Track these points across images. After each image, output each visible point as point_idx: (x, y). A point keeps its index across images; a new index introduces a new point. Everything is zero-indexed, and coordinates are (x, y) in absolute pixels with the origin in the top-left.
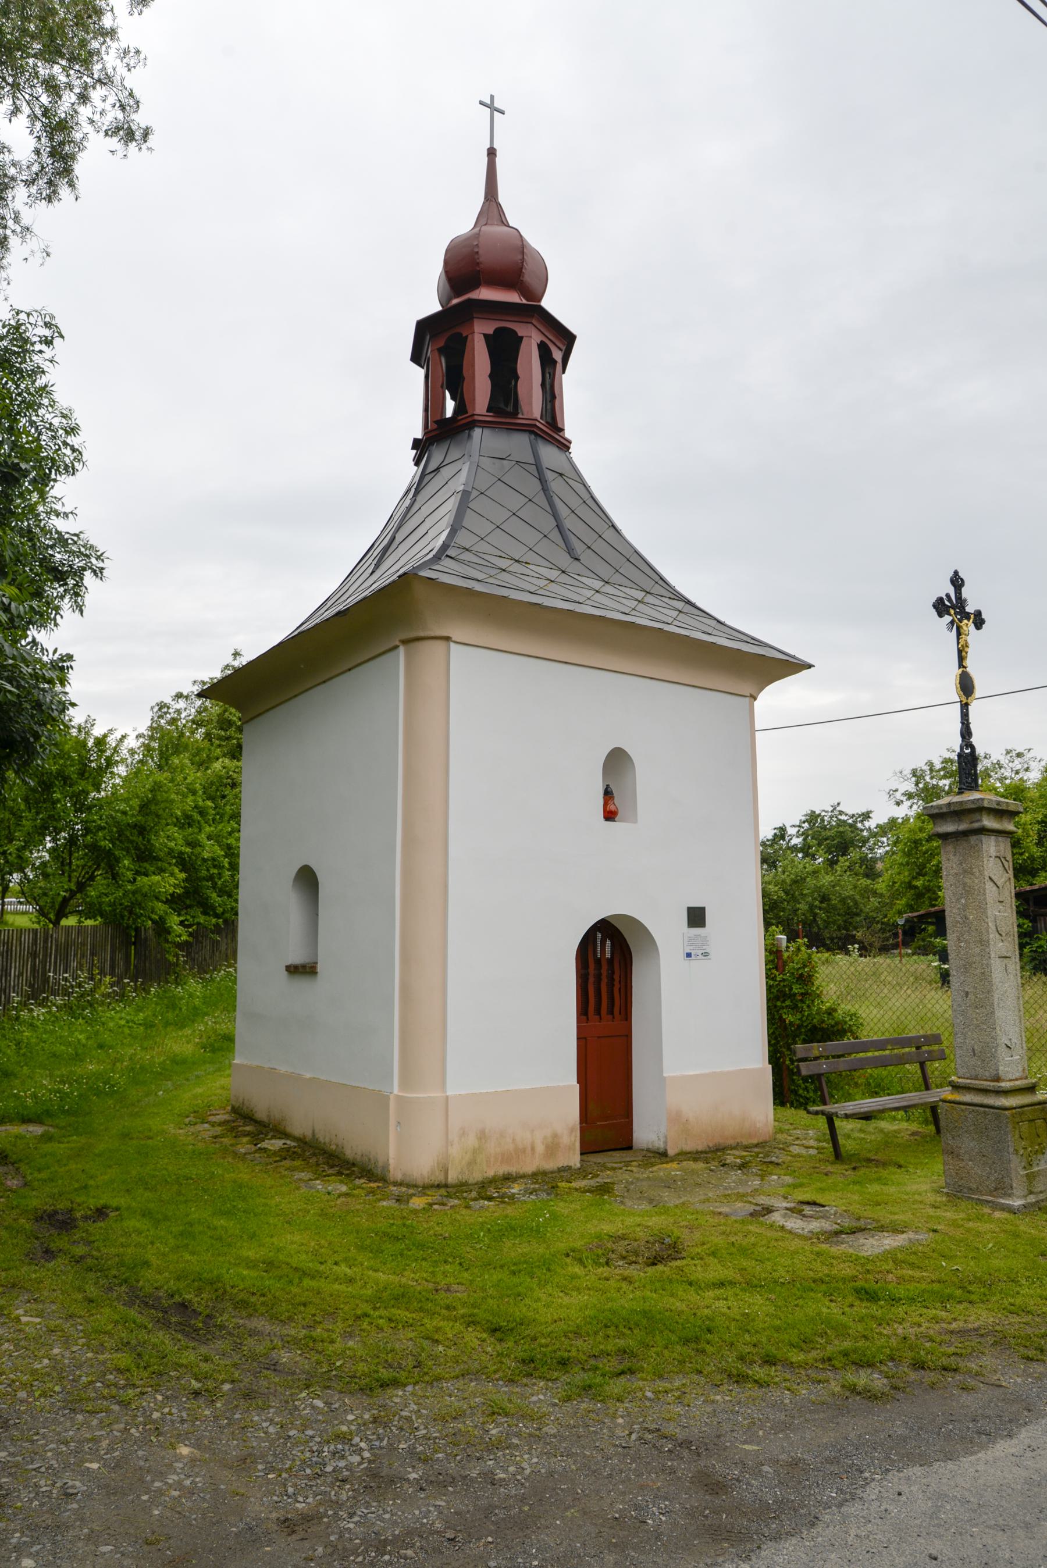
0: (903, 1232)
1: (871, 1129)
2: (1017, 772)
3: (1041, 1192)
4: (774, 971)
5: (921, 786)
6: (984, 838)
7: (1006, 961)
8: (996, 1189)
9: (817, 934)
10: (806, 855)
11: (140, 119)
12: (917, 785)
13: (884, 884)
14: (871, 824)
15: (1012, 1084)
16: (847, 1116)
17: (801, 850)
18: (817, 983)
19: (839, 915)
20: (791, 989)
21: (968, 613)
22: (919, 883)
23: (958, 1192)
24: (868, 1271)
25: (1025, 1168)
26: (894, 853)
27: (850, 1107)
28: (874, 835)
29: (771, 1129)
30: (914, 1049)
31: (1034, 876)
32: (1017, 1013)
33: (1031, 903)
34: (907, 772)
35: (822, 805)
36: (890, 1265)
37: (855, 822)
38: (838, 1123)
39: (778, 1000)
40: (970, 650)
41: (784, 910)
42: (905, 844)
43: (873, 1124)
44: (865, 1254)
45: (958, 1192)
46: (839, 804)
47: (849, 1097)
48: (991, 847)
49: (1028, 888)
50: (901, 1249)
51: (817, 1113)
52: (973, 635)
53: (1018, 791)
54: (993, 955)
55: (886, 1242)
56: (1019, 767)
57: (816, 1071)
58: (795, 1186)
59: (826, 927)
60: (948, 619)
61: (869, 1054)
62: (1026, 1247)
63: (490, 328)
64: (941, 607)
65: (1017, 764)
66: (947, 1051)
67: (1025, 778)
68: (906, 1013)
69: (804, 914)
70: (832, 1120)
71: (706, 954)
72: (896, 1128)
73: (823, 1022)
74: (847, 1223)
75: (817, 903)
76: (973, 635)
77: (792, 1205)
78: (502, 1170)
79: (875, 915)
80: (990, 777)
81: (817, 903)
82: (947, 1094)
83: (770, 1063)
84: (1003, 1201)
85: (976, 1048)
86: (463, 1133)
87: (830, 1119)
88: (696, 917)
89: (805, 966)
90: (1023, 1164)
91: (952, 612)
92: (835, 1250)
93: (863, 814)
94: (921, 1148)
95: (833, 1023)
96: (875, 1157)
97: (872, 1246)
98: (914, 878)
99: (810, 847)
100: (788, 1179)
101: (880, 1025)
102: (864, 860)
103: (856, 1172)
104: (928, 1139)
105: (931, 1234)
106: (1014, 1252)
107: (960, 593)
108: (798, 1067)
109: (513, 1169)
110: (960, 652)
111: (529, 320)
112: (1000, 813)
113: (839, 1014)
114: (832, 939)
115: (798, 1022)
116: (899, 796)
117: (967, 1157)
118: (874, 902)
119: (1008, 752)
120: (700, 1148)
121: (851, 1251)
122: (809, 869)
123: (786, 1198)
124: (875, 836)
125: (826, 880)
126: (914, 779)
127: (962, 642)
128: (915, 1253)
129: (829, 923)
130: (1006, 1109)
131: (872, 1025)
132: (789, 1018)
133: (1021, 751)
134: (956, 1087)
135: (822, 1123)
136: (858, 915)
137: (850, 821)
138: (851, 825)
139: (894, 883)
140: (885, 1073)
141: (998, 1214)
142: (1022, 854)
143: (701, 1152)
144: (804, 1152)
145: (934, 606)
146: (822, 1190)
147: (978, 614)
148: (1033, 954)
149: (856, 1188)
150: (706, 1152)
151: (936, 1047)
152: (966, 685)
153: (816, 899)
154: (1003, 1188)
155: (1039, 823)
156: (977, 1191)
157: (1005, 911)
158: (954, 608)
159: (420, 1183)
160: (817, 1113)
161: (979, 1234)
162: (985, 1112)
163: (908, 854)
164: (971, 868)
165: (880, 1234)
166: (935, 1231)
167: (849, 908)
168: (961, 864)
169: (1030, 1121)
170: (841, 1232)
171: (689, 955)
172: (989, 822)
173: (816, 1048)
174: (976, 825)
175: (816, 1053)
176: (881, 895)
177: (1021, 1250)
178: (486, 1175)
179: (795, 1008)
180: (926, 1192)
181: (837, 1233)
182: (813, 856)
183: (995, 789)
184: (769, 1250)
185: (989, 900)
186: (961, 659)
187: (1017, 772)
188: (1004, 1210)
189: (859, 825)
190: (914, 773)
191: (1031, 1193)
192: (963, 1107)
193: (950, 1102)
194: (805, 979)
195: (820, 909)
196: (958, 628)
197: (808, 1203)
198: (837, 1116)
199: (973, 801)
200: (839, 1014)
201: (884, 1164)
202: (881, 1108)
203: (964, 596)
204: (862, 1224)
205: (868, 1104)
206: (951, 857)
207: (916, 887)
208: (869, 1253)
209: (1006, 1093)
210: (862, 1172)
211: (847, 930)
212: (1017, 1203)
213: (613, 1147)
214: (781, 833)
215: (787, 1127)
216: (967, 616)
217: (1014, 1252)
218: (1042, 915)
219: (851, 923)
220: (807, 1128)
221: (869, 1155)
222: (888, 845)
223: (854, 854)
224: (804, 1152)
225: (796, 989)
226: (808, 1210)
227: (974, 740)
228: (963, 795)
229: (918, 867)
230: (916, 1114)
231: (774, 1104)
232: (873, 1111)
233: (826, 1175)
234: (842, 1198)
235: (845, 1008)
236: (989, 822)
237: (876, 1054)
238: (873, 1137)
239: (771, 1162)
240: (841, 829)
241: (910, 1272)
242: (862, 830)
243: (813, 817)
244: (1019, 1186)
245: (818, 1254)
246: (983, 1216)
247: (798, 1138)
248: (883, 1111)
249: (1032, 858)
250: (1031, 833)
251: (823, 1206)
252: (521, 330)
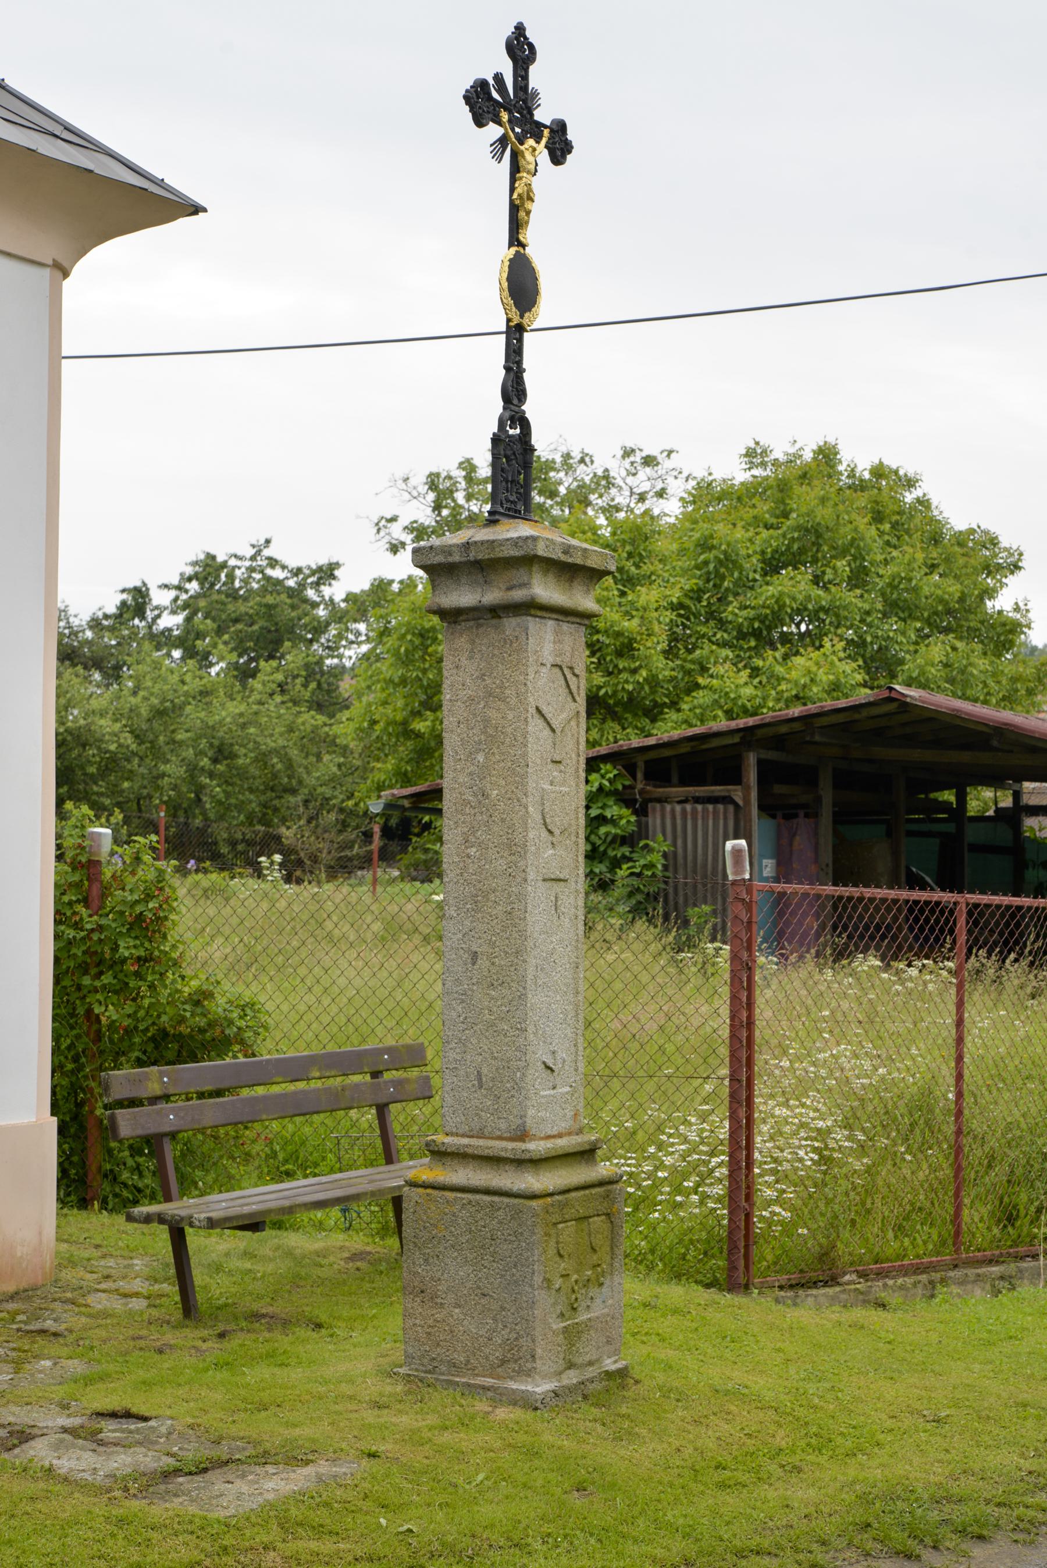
0: (307, 1462)
1: (266, 1251)
2: (642, 498)
3: (591, 1363)
4: (80, 908)
5: (445, 512)
6: (532, 624)
7: (558, 887)
8: (503, 1362)
9: (202, 832)
10: (190, 652)
12: (437, 507)
13: (352, 726)
14: (337, 591)
15: (549, 1144)
16: (212, 1224)
17: (180, 642)
18: (172, 936)
19: (251, 790)
20: (115, 948)
21: (539, 125)
22: (421, 726)
23: (428, 1372)
24: (225, 1549)
25: (562, 1315)
26: (378, 658)
27: (221, 1203)
28: (339, 616)
29: (48, 1260)
30: (368, 1077)
31: (654, 720)
32: (571, 998)
33: (640, 776)
34: (419, 480)
35: (231, 544)
36: (274, 1533)
37: (302, 586)
38: (194, 1239)
39: (86, 972)
40: (535, 208)
41: (130, 776)
42: (402, 637)
43: (268, 1240)
44: (220, 1514)
45: (428, 1372)
46: (268, 542)
47: (227, 1183)
48: (547, 644)
49: (636, 742)
50: (300, 1497)
51: (148, 1219)
52: (546, 178)
53: (637, 538)
54: (532, 875)
55: (270, 1485)
56: (645, 486)
57: (152, 1128)
58: (88, 1381)
59: (221, 818)
60: (494, 131)
61: (275, 1089)
62: (550, 1476)
64: (481, 102)
65: (642, 480)
66: (436, 1081)
67: (656, 512)
68: (358, 1002)
69: (175, 787)
70: (181, 1232)
72: (319, 1245)
73: (182, 1020)
74: (193, 1452)
75: (205, 762)
76: (546, 178)
77: (77, 1421)
79: (327, 791)
80: (589, 504)
81: (205, 762)
82: (424, 1170)
83: (55, 1110)
84: (514, 1385)
85: (485, 1071)
87: (178, 1237)
89: (148, 897)
90: (559, 1309)
91: (505, 116)
92: (158, 1511)
93: (320, 569)
94: (367, 1286)
95: (203, 1022)
96: (270, 1310)
97: (239, 1496)
98: (416, 714)
99: (200, 635)
100: (75, 1366)
101: (302, 1026)
102: (313, 671)
103: (226, 1344)
104: (383, 1267)
105: (364, 1462)
106: (525, 1486)
107: (525, 78)
108: (112, 1119)
110: (515, 209)
112: (571, 571)
113: (218, 1006)
114: (233, 843)
115: (126, 1022)
116: (397, 532)
117: (451, 1298)
118: (330, 763)
119: (628, 453)
121: (193, 1509)
122: (194, 685)
123: (64, 1406)
124: (340, 620)
125: (228, 711)
126: (431, 496)
127: (520, 188)
128: (326, 1504)
129: (228, 808)
130: (534, 1197)
131: (286, 1026)
132: (109, 1013)
133: (654, 451)
134: (440, 1154)
135: (161, 1239)
136: (293, 792)
137: (291, 583)
138: (291, 593)
139: (374, 722)
140: (307, 1130)
141: (502, 1413)
142: (634, 671)
144: (117, 1305)
145: (467, 99)
146: (147, 1384)
147: (559, 128)
148: (635, 882)
149: (219, 1376)
151: (414, 1073)
152: (522, 287)
153: (202, 753)
154: (516, 1359)
155: (673, 607)
156: (468, 1367)
157: (563, 783)
158: (505, 105)
160: (148, 1219)
161: (461, 1456)
162: (492, 1205)
163: (406, 660)
164: (502, 687)
165: (258, 1469)
166: (373, 1455)
167: (275, 776)
168: (482, 677)
169: (580, 1219)
170: (177, 1472)
172: (545, 590)
173: (156, 1079)
174: (518, 595)
175: (154, 1088)
176: (345, 750)
177: (540, 1482)
179: (121, 990)
180: (364, 1376)
181: (167, 1475)
182: (206, 655)
183: (594, 529)
184: (14, 1523)
185: (533, 757)
186: (516, 224)
187: (642, 498)
188: (514, 1403)
189: (311, 593)
190: (433, 482)
191: (571, 1365)
193: (425, 1186)
194: (147, 926)
195: (211, 775)
196: (515, 156)
197: (113, 1415)
198: (191, 1225)
199: (516, 542)
200: (218, 1006)
201: (286, 1323)
202: (287, 1203)
203: (533, 82)
204: (223, 1452)
205: (257, 1195)
206: (464, 662)
207: (418, 735)
208: (232, 1511)
209: (536, 1163)
210: (233, 1343)
211: (268, 824)
212: (541, 1387)
214: (138, 601)
215: (86, 1254)
216: (535, 130)
217: (525, 1486)
218: (659, 800)
219: (276, 810)
220: (130, 1253)
221: (255, 1307)
222: (368, 640)
223: (293, 658)
224: (117, 1305)
225: (127, 948)
226: (110, 1430)
227: (529, 408)
228: (498, 528)
229: (425, 689)
230: (366, 1215)
231: (62, 1202)
232: (269, 1211)
233: (160, 1352)
234: (188, 1395)
235: (228, 993)
236: (545, 590)
237: (292, 1087)
238: (270, 1268)
239: (43, 1332)
240: (270, 599)
241: (313, 1545)
242: (315, 605)
243: (209, 570)
244: (547, 1354)
245: (121, 1522)
246: (472, 1418)
247: (107, 1277)
248: (290, 1210)
249: (653, 682)
250: (656, 628)
251: (146, 1419)
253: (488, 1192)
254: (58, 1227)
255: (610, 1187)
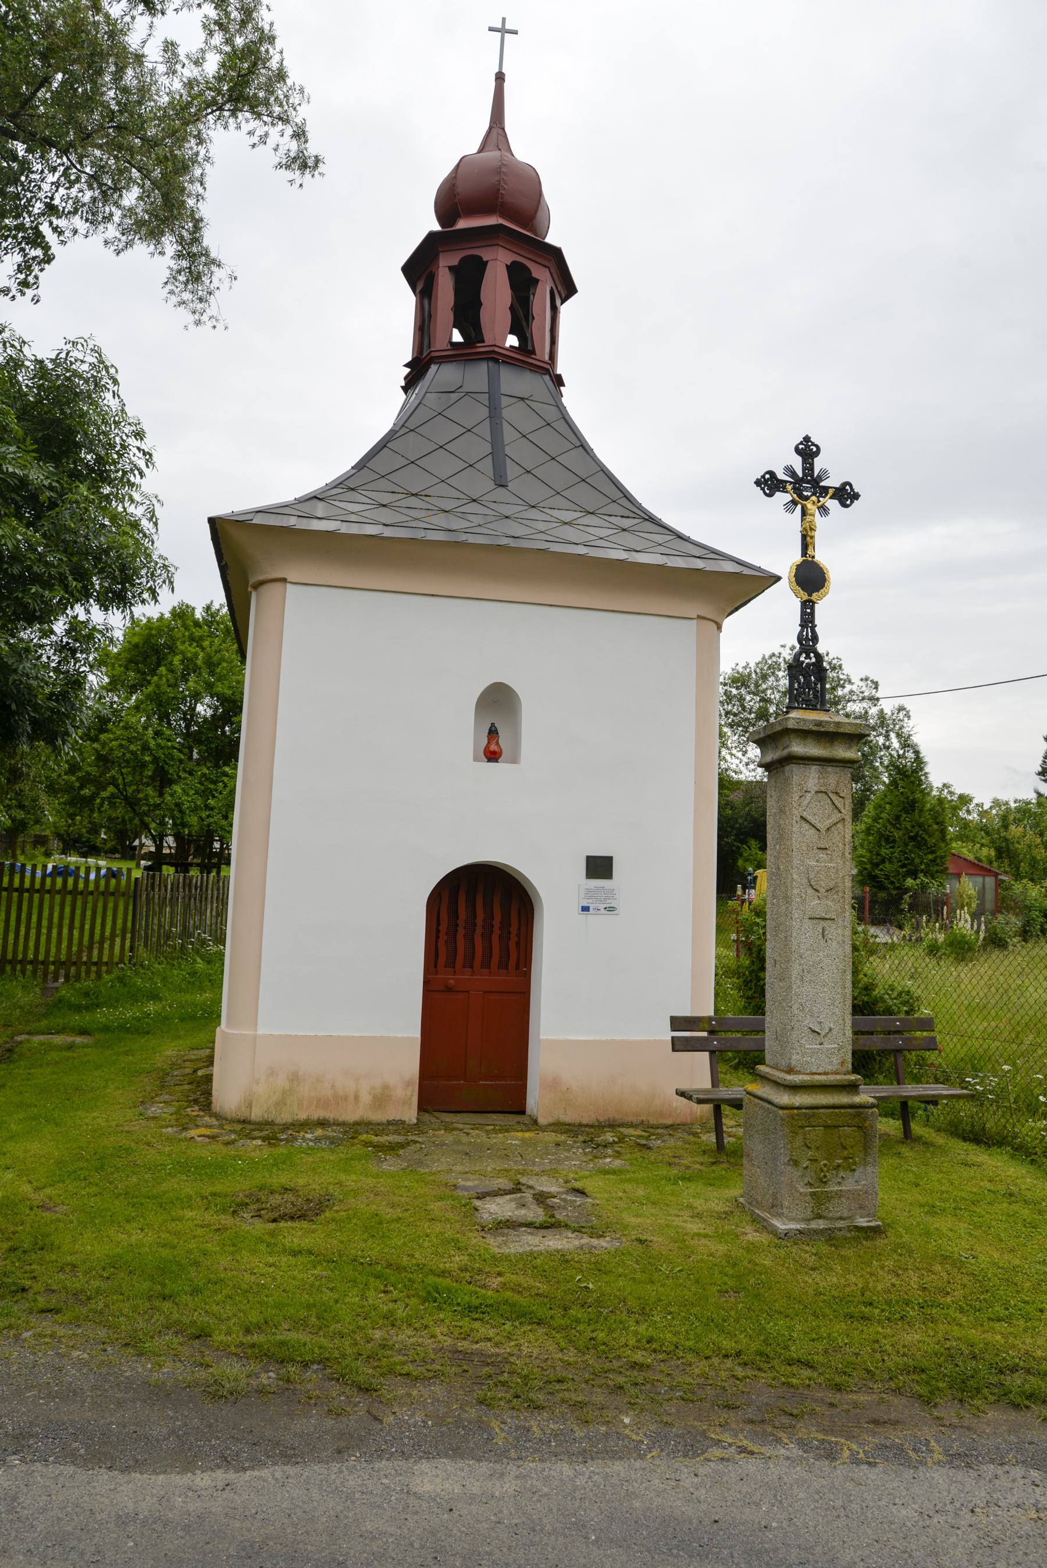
7: (825, 924)
11: (312, 149)
40: (817, 535)
63: (454, 259)
71: (611, 909)
78: (317, 1114)
86: (272, 1073)
88: (599, 867)
109: (330, 1115)
110: (804, 537)
111: (495, 242)
120: (585, 1121)
143: (586, 1126)
150: (592, 1126)
159: (229, 1117)
169: (826, 1127)
171: (585, 909)
172: (798, 748)
178: (296, 1117)
192: (757, 1101)
212: (780, 1225)
213: (499, 1109)
252: (486, 254)
253: (834, 1107)
254: (210, 1061)
255: (861, 1110)
